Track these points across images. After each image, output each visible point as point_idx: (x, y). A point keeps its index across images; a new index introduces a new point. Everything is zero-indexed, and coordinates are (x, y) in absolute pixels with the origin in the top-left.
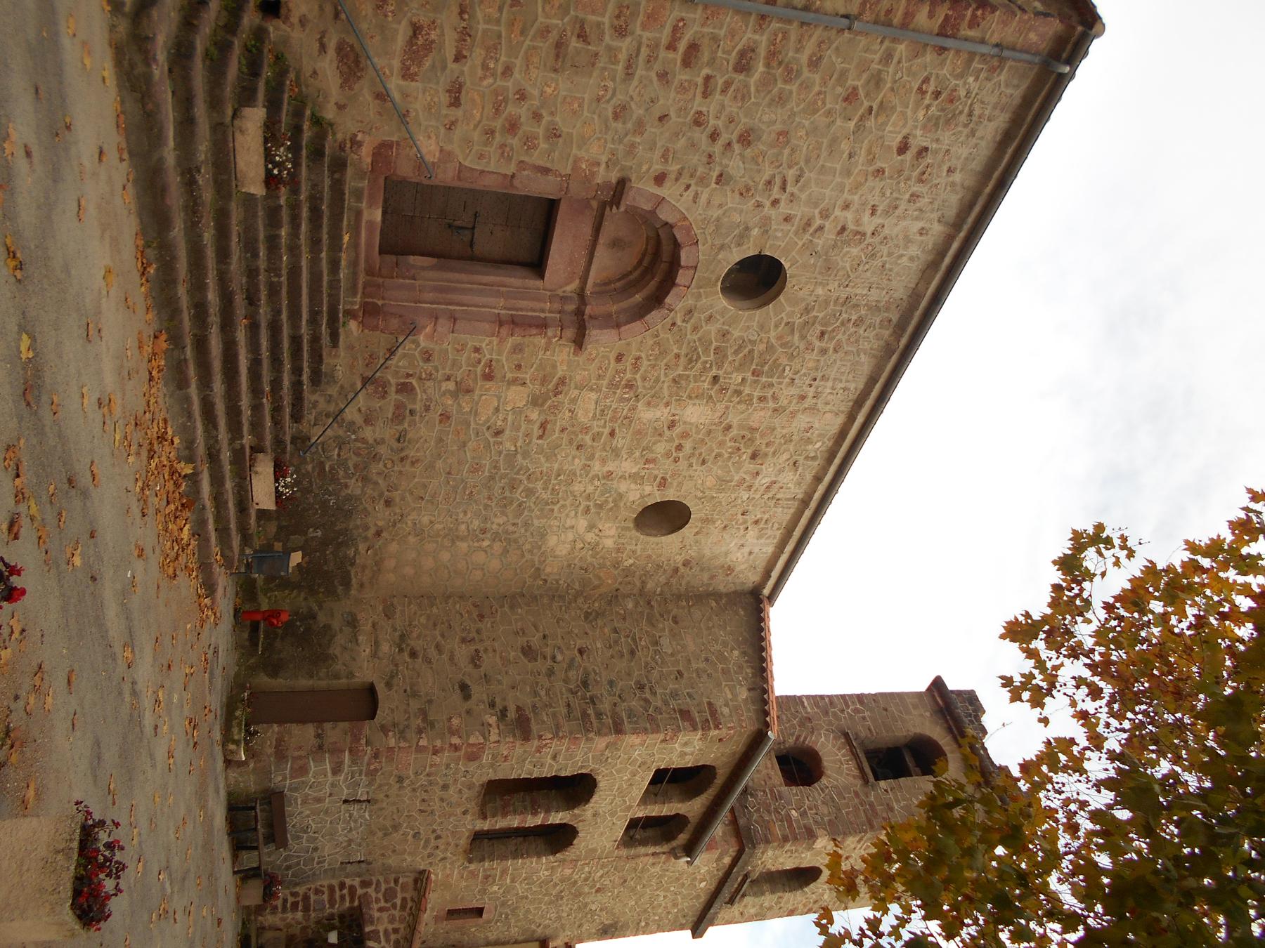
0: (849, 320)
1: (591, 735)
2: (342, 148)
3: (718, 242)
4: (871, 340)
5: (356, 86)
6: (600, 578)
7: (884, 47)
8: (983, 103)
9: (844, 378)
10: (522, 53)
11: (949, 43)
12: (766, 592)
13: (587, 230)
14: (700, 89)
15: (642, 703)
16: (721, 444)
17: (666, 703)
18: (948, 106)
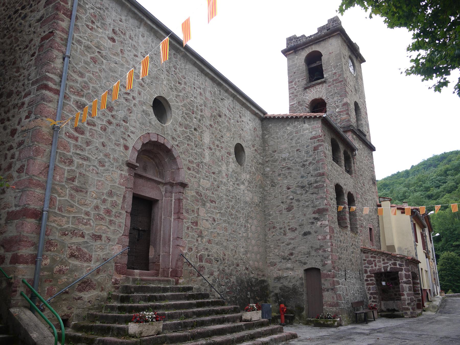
0: (174, 71)
1: (325, 185)
2: (118, 288)
3: (148, 124)
4: (181, 64)
5: (95, 282)
6: (259, 181)
7: (75, 43)
8: (96, 3)
9: (194, 76)
10: (80, 207)
11: (74, 13)
12: (262, 115)
14: (92, 127)
15: (311, 165)
16: (216, 129)
17: (311, 156)
18: (97, 18)
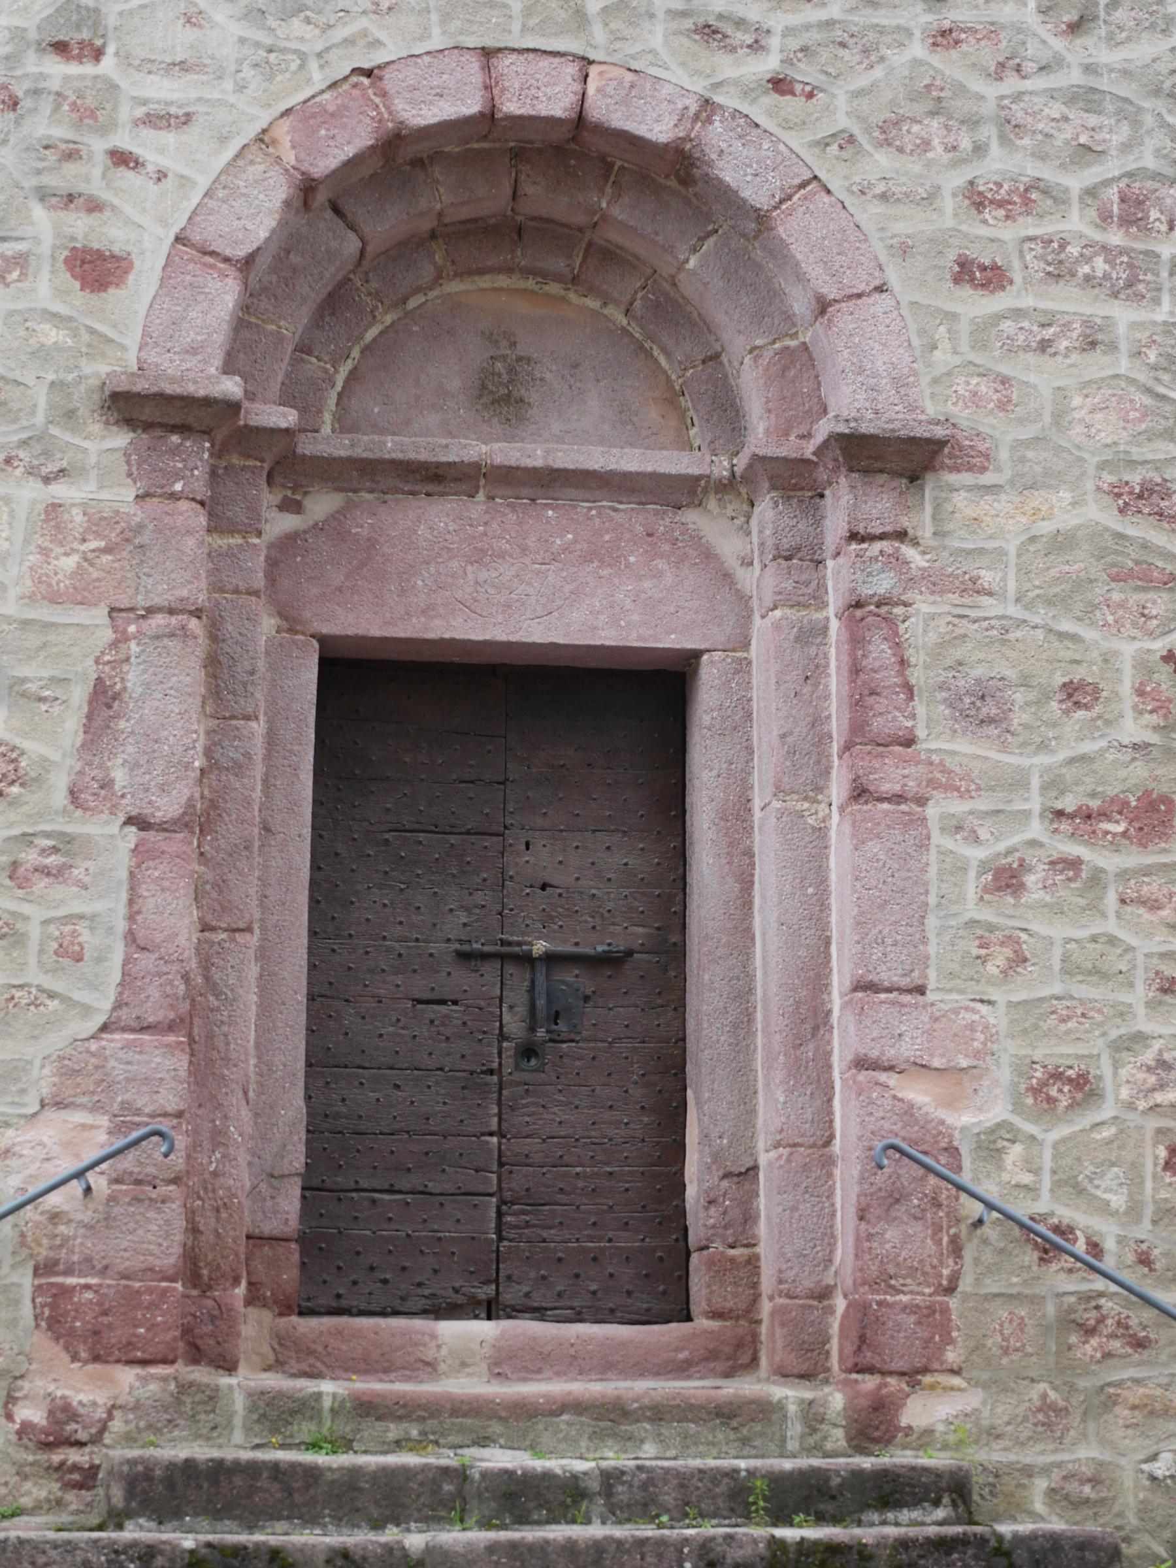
13: (438, 519)
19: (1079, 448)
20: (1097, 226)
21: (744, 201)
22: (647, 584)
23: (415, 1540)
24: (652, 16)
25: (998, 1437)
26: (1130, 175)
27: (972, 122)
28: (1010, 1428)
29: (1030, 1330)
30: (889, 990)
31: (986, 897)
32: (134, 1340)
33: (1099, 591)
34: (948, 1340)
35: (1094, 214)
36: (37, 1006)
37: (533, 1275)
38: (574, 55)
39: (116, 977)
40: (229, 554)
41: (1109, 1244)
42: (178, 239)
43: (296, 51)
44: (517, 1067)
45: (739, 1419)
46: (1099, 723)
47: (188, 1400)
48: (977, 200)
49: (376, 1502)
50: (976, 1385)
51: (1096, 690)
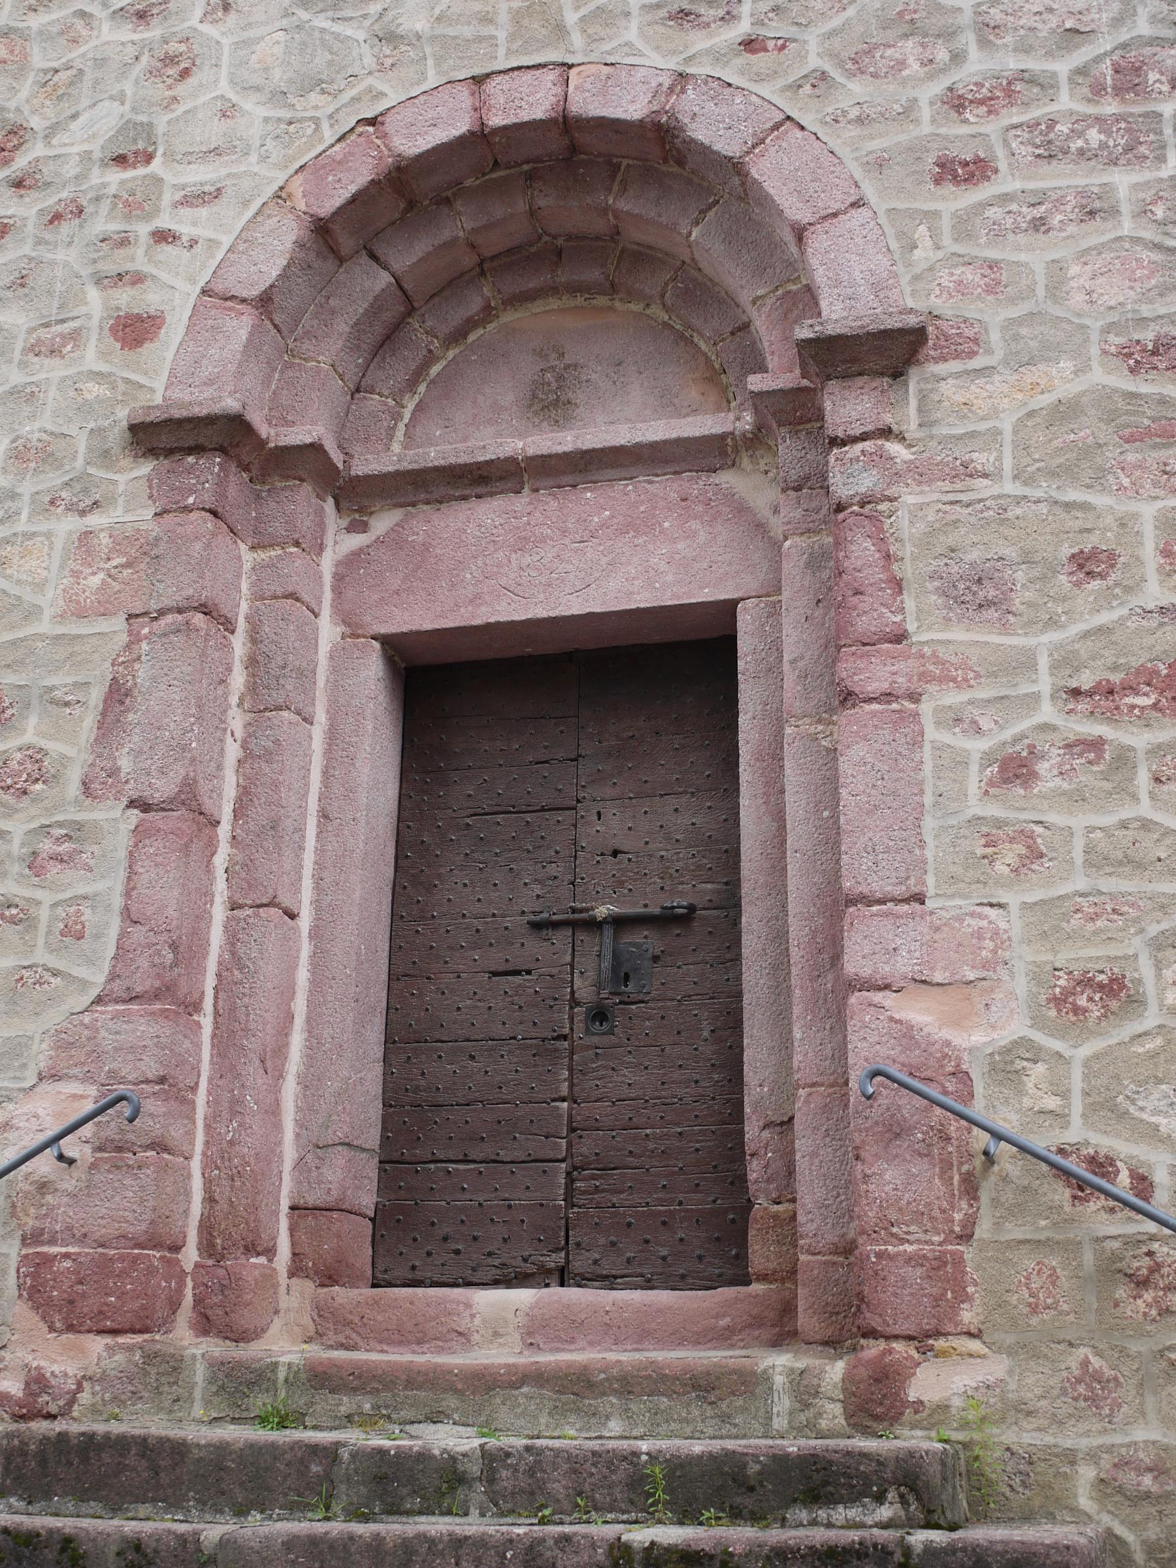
19: (1079, 315)
20: (1089, 101)
21: (718, 153)
22: (681, 546)
23: (213, 1531)
24: (627, 14)
25: (1029, 1413)
26: (1124, 46)
27: (948, 34)
28: (1043, 1403)
29: (1064, 1283)
30: (881, 902)
31: (992, 791)
32: (105, 1308)
33: (1111, 455)
34: (962, 1297)
35: (1086, 90)
36: (41, 984)
37: (602, 1241)
38: (553, 64)
39: (111, 951)
40: (271, 565)
41: (1160, 1177)
42: (204, 292)
43: (311, 118)
44: (588, 1032)
45: (717, 1392)
46: (1117, 590)
47: (154, 1371)
48: (956, 103)
49: (242, 1484)
50: (999, 1351)
51: (1112, 558)
